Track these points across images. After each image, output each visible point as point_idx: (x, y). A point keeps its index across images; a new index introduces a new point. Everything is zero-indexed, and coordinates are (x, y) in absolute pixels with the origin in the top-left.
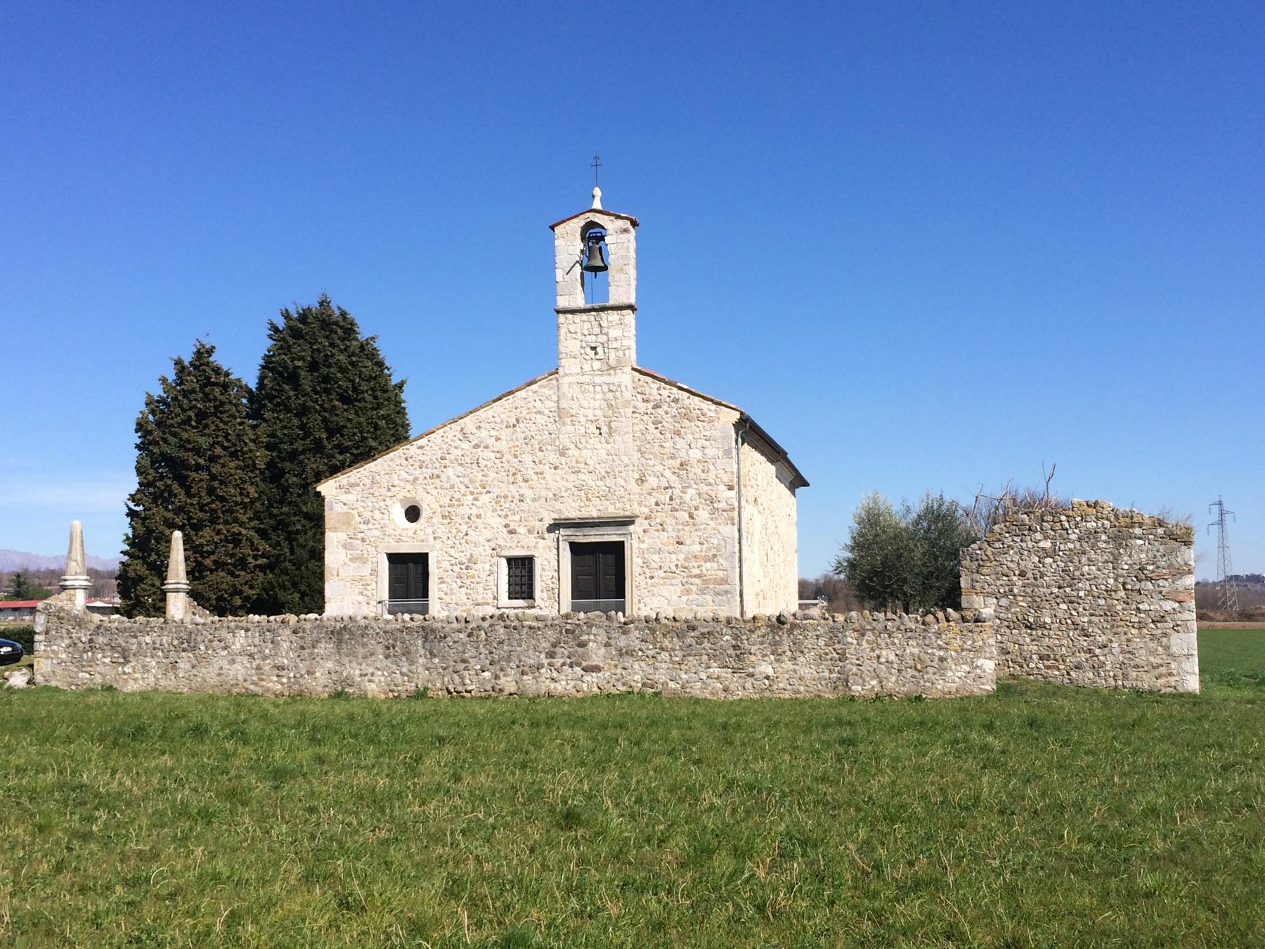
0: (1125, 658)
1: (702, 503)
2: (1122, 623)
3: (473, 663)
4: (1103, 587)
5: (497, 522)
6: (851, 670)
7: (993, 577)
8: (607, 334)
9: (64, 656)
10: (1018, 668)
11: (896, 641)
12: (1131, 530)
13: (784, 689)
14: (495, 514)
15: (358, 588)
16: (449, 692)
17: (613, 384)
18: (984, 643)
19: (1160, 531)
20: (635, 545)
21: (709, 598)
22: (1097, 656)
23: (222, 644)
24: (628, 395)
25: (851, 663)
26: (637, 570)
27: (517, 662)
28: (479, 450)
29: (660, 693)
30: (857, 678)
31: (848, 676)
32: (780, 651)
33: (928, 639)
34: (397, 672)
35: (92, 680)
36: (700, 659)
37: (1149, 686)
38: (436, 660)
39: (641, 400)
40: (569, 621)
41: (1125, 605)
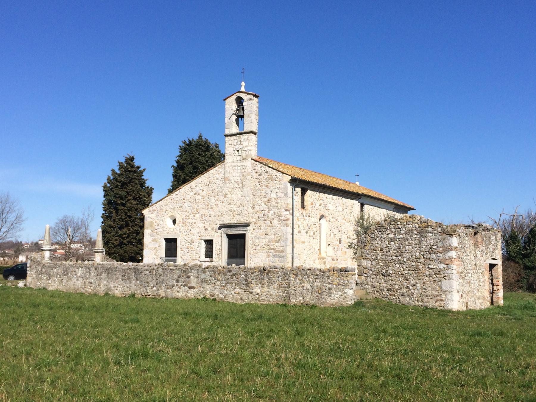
0: (422, 291)
1: (275, 217)
2: (422, 274)
3: (150, 284)
4: (414, 257)
7: (370, 251)
8: (242, 144)
9: (34, 276)
10: (379, 294)
11: (311, 280)
12: (427, 229)
13: (264, 300)
14: (201, 222)
15: (154, 252)
16: (142, 296)
17: (244, 166)
18: (348, 282)
19: (439, 229)
21: (276, 258)
22: (411, 290)
23: (75, 273)
24: (249, 170)
25: (292, 289)
26: (250, 246)
27: (165, 283)
28: (196, 195)
29: (215, 299)
30: (294, 296)
31: (290, 295)
32: (263, 282)
34: (126, 286)
35: (41, 285)
36: (232, 285)
37: (432, 305)
38: (138, 282)
39: (254, 172)
40: (185, 267)
41: (423, 266)
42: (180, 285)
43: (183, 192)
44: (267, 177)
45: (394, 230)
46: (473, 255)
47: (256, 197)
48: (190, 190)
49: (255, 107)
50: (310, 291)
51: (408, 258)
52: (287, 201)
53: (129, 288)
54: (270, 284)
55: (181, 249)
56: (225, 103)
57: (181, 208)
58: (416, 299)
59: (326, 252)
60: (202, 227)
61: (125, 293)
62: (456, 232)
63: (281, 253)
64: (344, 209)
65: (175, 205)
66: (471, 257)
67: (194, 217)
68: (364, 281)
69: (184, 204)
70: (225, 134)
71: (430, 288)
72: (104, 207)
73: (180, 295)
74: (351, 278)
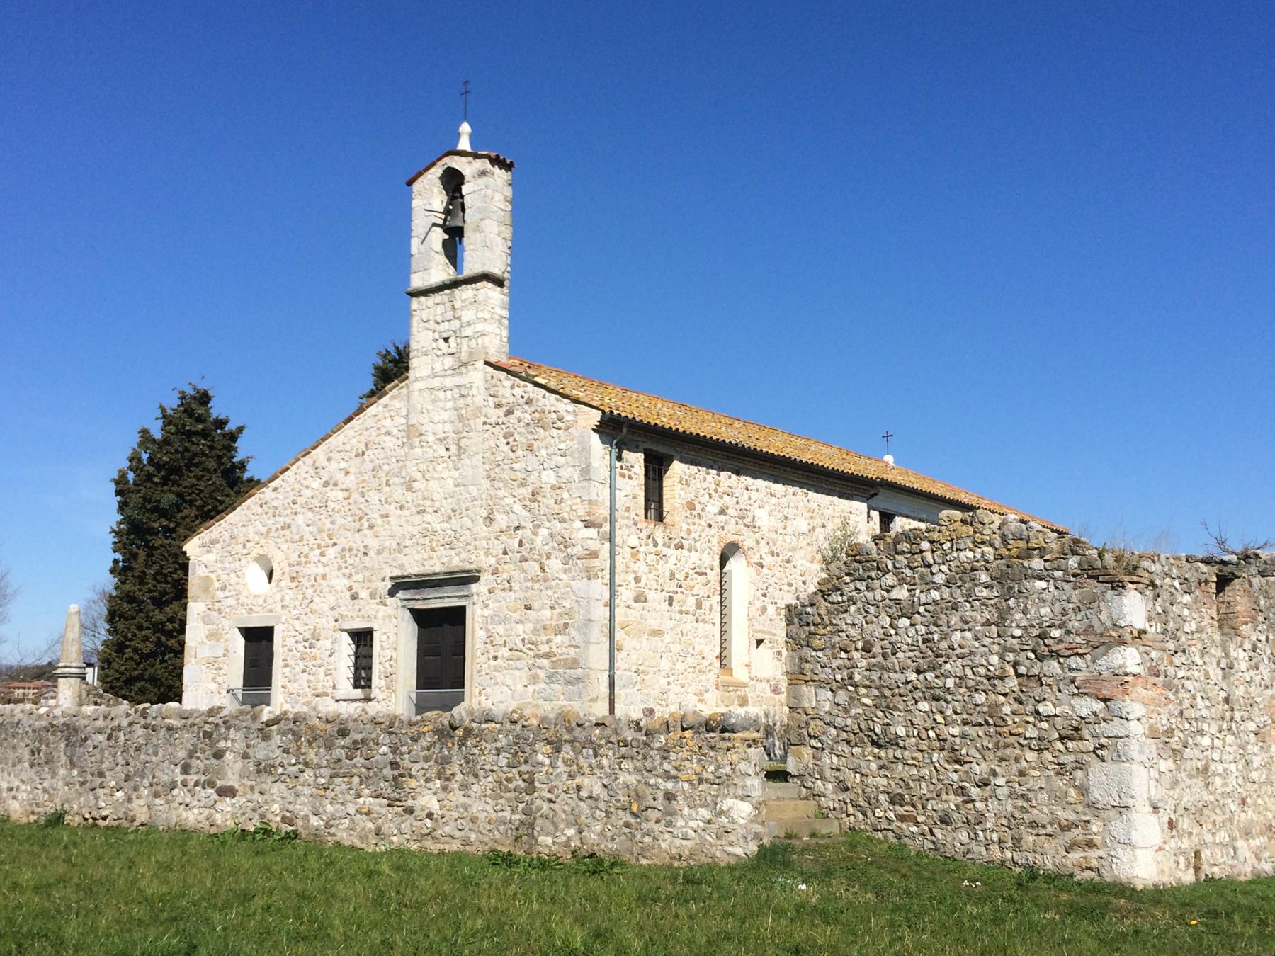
0: (1016, 808)
2: (1012, 740)
3: (109, 778)
4: (982, 671)
5: (341, 583)
6: (540, 809)
8: (459, 318)
10: (861, 817)
11: (605, 761)
12: (1026, 563)
16: (86, 819)
19: (1073, 562)
20: (479, 612)
21: (556, 687)
22: (973, 801)
24: (479, 400)
25: (541, 798)
26: (480, 645)
28: (328, 489)
30: (548, 824)
31: (535, 819)
32: (448, 772)
33: (650, 760)
34: (40, 787)
37: (1054, 864)
38: (75, 772)
39: (492, 405)
40: (211, 719)
41: (1016, 706)
42: (192, 783)
43: (291, 480)
44: (529, 417)
45: (908, 572)
46: (1218, 663)
47: (497, 484)
48: (312, 472)
49: (498, 197)
50: (602, 805)
51: (960, 678)
52: (589, 493)
53: (49, 793)
54: (471, 779)
55: (284, 660)
56: (412, 192)
57: (287, 532)
58: (995, 836)
59: (748, 666)
60: (344, 590)
61: (37, 810)
62: (1139, 572)
63: (571, 668)
64: (814, 529)
65: (271, 522)
66: (1207, 673)
67: (323, 559)
68: (810, 765)
69: (296, 517)
70: (409, 289)
71: (1043, 796)
72: (116, 540)
73: (192, 818)
74: (744, 756)
